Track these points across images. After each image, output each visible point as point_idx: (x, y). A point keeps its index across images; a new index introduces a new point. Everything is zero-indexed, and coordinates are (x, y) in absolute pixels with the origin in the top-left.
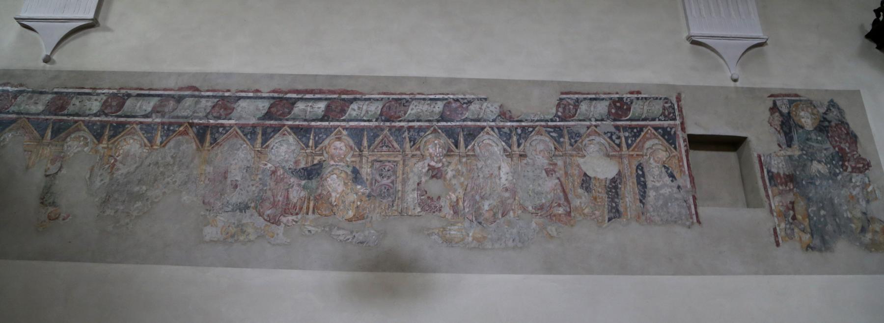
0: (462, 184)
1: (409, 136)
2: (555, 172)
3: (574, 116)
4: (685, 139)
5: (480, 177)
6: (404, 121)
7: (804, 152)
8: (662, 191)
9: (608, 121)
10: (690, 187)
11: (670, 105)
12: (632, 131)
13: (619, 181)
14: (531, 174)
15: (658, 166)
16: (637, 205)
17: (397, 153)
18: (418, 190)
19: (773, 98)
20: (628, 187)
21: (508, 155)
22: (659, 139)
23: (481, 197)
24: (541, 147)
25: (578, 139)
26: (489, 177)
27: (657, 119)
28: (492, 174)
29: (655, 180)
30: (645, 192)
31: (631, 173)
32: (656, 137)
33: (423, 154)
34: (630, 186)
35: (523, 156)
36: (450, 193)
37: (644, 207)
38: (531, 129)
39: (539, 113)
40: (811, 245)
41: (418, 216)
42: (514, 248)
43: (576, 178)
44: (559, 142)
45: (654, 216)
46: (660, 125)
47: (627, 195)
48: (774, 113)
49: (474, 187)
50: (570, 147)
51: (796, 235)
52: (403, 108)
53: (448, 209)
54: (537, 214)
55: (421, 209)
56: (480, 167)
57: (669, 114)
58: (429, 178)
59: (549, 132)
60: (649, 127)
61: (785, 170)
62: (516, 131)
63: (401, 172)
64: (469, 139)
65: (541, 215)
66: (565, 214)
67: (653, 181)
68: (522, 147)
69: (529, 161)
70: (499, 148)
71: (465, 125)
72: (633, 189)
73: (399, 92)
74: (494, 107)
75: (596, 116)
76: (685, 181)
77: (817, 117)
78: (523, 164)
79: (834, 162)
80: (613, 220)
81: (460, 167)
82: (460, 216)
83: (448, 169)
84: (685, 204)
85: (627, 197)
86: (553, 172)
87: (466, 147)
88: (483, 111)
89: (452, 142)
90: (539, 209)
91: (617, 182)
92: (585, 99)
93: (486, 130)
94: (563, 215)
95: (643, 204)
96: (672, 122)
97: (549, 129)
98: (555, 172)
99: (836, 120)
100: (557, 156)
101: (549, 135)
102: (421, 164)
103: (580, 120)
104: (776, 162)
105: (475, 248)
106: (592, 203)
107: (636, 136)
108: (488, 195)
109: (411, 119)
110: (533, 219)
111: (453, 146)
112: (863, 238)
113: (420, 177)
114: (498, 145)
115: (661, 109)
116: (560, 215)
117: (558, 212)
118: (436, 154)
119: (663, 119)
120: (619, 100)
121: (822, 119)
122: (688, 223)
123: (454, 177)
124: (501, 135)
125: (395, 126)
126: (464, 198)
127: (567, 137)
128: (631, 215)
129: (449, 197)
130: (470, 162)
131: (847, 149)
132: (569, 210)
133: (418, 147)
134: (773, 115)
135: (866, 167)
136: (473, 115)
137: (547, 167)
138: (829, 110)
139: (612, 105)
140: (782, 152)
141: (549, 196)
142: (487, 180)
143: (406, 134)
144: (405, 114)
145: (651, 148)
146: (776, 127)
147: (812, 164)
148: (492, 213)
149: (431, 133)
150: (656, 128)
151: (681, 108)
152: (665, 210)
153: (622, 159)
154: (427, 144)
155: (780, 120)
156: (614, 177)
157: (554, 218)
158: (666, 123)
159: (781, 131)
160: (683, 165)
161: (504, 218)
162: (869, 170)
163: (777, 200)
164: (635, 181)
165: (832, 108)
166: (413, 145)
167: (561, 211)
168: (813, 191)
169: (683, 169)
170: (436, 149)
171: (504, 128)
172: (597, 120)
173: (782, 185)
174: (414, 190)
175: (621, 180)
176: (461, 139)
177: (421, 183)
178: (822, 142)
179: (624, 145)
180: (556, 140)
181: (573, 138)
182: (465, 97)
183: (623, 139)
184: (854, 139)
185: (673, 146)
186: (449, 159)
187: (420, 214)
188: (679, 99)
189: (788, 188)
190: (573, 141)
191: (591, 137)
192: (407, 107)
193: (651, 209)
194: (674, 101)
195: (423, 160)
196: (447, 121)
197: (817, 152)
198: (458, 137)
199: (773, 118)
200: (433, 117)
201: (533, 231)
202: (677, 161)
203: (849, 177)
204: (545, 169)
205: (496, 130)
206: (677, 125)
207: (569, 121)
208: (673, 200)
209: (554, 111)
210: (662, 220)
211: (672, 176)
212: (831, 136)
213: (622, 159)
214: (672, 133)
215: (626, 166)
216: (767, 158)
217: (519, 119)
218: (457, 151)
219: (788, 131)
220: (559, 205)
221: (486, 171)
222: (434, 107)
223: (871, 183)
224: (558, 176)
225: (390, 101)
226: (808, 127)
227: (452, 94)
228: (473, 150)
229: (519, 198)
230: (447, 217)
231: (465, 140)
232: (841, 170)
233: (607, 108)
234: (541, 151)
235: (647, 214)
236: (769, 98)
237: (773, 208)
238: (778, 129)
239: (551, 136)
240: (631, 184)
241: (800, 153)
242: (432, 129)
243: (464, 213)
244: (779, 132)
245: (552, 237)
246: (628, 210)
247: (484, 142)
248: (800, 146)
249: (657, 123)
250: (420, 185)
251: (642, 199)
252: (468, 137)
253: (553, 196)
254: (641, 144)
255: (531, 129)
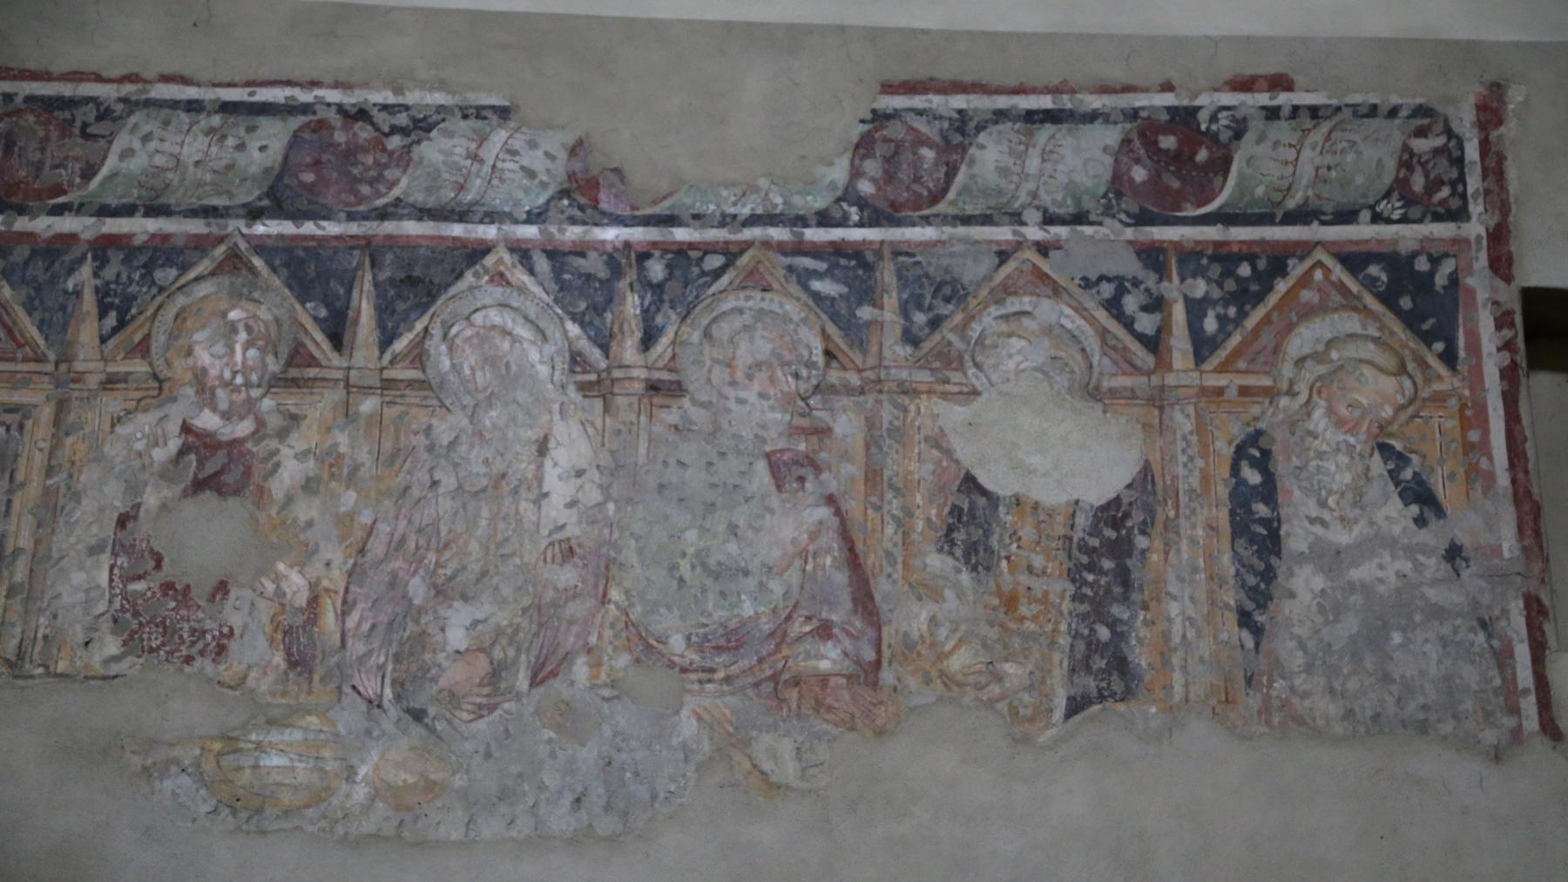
0: (345, 522)
1: (98, 282)
2: (817, 469)
3: (935, 199)
4: (1509, 313)
5: (441, 490)
6: (79, 209)
8: (1362, 572)
9: (1108, 221)
10: (1517, 553)
11: (1440, 141)
12: (1229, 273)
13: (1138, 517)
14: (695, 478)
15: (1351, 447)
16: (1224, 636)
17: (32, 366)
18: (119, 548)
20: (1184, 545)
21: (591, 383)
22: (1366, 311)
23: (434, 585)
24: (762, 346)
25: (945, 309)
26: (484, 490)
27: (1365, 215)
28: (503, 476)
29: (1326, 515)
30: (1269, 575)
31: (1205, 479)
32: (1351, 304)
33: (164, 372)
34: (1193, 541)
35: (661, 390)
36: (281, 567)
37: (1257, 645)
38: (714, 262)
39: (763, 183)
41: (104, 678)
42: (579, 840)
43: (919, 499)
44: (849, 326)
45: (1305, 695)
46: (1379, 242)
47: (1173, 587)
49: (403, 540)
50: (905, 351)
52: (77, 147)
53: (262, 643)
54: (712, 671)
55: (125, 644)
56: (445, 439)
57: (1433, 185)
58: (178, 489)
59: (804, 277)
60: (1320, 255)
62: (641, 269)
63: (39, 459)
64: (401, 306)
65: (728, 680)
66: (849, 677)
67: (1313, 521)
68: (663, 344)
69: (696, 414)
70: (549, 349)
71: (389, 237)
72: (1211, 558)
73: (65, 68)
74: (540, 153)
75: (1046, 199)
76: (1491, 524)
78: (658, 429)
80: (1096, 708)
81: (342, 440)
82: (316, 677)
83: (285, 451)
84: (1481, 637)
85: (1175, 598)
86: (808, 472)
87: (386, 341)
88: (487, 169)
89: (315, 319)
90: (719, 649)
91: (1129, 524)
92: (1000, 115)
93: (489, 261)
94: (843, 681)
95: (1258, 632)
96: (1442, 230)
97: (807, 262)
98: (817, 469)
100: (832, 389)
101: (806, 288)
102: (146, 421)
103: (967, 220)
105: (376, 837)
106: (992, 625)
107: (1245, 297)
108: (472, 577)
109: (113, 201)
110: (687, 698)
111: (319, 337)
113: (134, 489)
114: (545, 338)
115: (1391, 165)
116: (824, 679)
117: (812, 663)
118: (227, 375)
119: (1396, 216)
120: (1172, 120)
122: (1489, 736)
123: (310, 486)
124: (563, 287)
125: (30, 236)
126: (347, 590)
127: (891, 301)
128: (1186, 685)
129: (270, 587)
130: (401, 416)
132: (869, 655)
133: (137, 338)
136: (429, 190)
137: (782, 445)
139: (1137, 143)
141: (777, 588)
142: (472, 505)
143: (86, 271)
144: (89, 173)
145: (1318, 357)
148: (482, 665)
149: (212, 274)
150: (1354, 260)
151: (1501, 158)
152: (1369, 663)
153: (1161, 409)
154: (189, 323)
156: (1117, 501)
157: (793, 694)
158: (1406, 236)
160: (1484, 447)
161: (542, 689)
164: (1223, 517)
166: (115, 330)
167: (829, 658)
169: (1484, 463)
170: (232, 352)
171: (582, 254)
172: (1049, 220)
174: (94, 551)
175: (1152, 513)
176: (364, 305)
177: (135, 518)
179: (1180, 343)
180: (835, 318)
181: (920, 308)
182: (400, 100)
183: (1179, 313)
185: (1439, 346)
186: (291, 401)
187: (114, 669)
188: (1490, 113)
190: (920, 318)
191: (1009, 300)
192: (102, 142)
193: (1299, 660)
194: (1465, 120)
195: (160, 406)
196: (298, 216)
198: (349, 291)
200: (230, 195)
201: (681, 755)
202: (1452, 424)
204: (768, 456)
205: (542, 264)
206: (1467, 241)
207: (913, 225)
208: (1418, 618)
209: (839, 173)
210: (1349, 714)
211: (1421, 496)
213: (1161, 409)
214: (1440, 280)
215: (1180, 445)
217: (662, 209)
218: (336, 360)
220: (825, 631)
221: (476, 462)
222: (241, 147)
224: (833, 487)
225: (18, 112)
227: (336, 85)
228: (418, 356)
229: (627, 592)
230: (250, 682)
231: (384, 310)
233: (1109, 160)
234: (759, 365)
235: (1270, 686)
239: (817, 297)
240: (1200, 532)
242: (220, 251)
243: (338, 665)
245: (774, 788)
246: (1176, 660)
247: (478, 318)
249: (1362, 231)
250: (130, 525)
251: (1250, 606)
252: (399, 296)
253: (796, 590)
254: (1267, 339)
255: (714, 262)
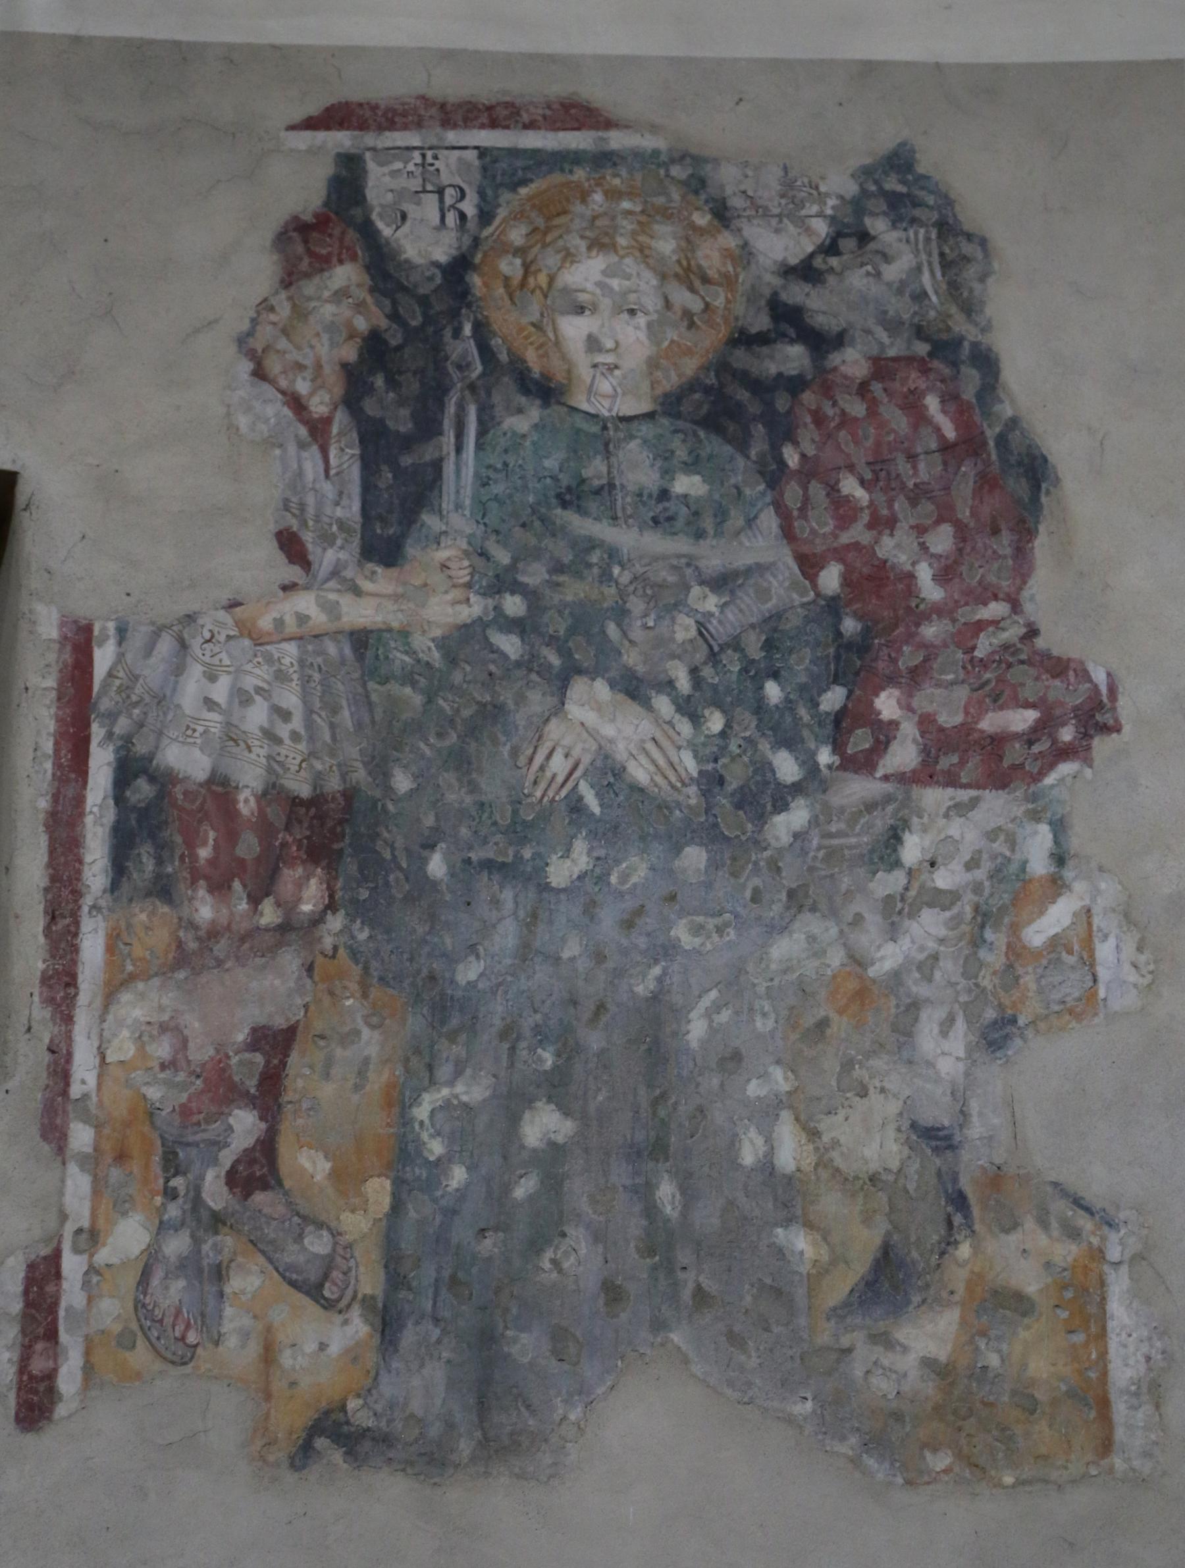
7: (514, 605)
19: (342, 140)
40: (359, 1414)
48: (322, 263)
51: (233, 1320)
61: (292, 753)
77: (719, 302)
79: (773, 691)
99: (893, 326)
104: (220, 691)
112: (864, 1354)
121: (761, 322)
131: (924, 573)
134: (309, 288)
135: (1067, 734)
138: (848, 244)
140: (306, 603)
146: (302, 387)
147: (559, 709)
155: (361, 324)
159: (341, 419)
162: (1088, 762)
163: (138, 1013)
165: (878, 225)
168: (507, 936)
173: (220, 887)
178: (708, 524)
184: (1019, 487)
189: (269, 915)
197: (636, 605)
199: (300, 313)
203: (881, 821)
212: (810, 471)
216: (149, 650)
219: (402, 422)
223: (1068, 874)
226: (605, 386)
232: (825, 757)
236: (304, 140)
237: (75, 1091)
238: (319, 406)
241: (477, 607)
244: (318, 430)
248: (484, 554)
